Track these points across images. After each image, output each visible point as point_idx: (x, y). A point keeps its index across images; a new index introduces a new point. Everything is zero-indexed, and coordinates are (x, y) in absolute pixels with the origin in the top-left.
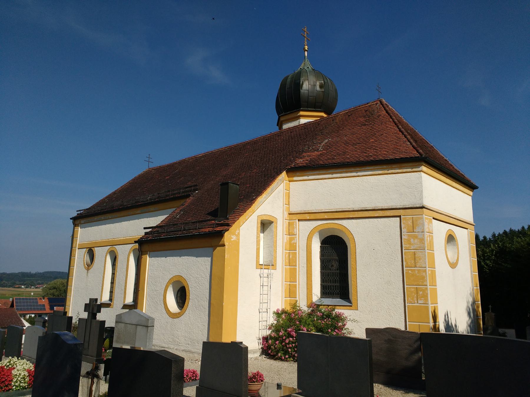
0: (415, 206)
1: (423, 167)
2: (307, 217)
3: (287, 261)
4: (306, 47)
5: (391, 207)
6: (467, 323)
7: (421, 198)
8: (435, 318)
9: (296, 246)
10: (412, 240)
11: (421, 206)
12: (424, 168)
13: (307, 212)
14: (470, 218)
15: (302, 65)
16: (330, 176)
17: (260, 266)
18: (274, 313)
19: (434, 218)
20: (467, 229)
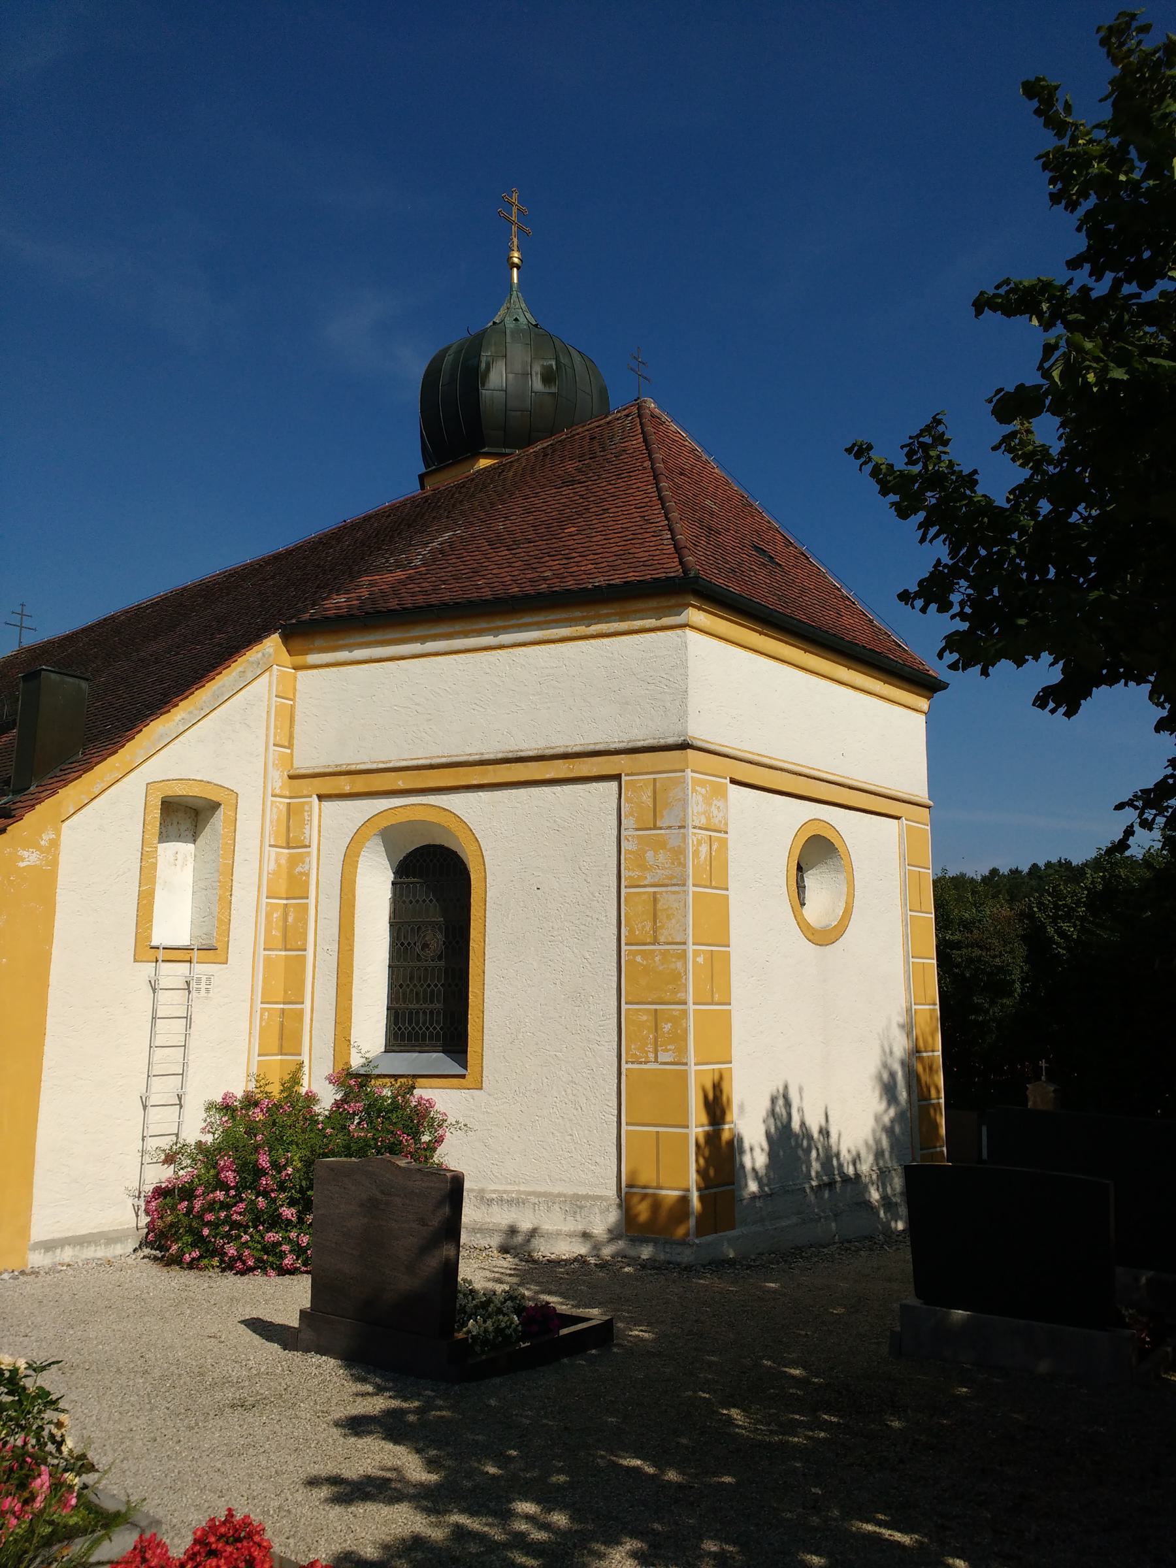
0: (662, 742)
1: (691, 610)
2: (345, 785)
3: (277, 933)
4: (516, 254)
5: (591, 748)
6: (877, 1119)
7: (683, 716)
8: (716, 1107)
9: (307, 883)
10: (650, 855)
11: (680, 740)
12: (694, 615)
13: (344, 768)
14: (919, 789)
15: (502, 311)
16: (416, 648)
17: (149, 951)
18: (210, 1106)
19: (733, 781)
20: (898, 818)
